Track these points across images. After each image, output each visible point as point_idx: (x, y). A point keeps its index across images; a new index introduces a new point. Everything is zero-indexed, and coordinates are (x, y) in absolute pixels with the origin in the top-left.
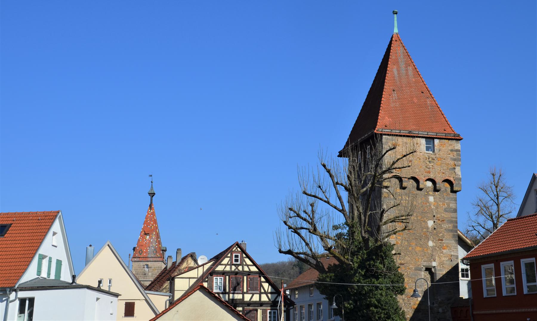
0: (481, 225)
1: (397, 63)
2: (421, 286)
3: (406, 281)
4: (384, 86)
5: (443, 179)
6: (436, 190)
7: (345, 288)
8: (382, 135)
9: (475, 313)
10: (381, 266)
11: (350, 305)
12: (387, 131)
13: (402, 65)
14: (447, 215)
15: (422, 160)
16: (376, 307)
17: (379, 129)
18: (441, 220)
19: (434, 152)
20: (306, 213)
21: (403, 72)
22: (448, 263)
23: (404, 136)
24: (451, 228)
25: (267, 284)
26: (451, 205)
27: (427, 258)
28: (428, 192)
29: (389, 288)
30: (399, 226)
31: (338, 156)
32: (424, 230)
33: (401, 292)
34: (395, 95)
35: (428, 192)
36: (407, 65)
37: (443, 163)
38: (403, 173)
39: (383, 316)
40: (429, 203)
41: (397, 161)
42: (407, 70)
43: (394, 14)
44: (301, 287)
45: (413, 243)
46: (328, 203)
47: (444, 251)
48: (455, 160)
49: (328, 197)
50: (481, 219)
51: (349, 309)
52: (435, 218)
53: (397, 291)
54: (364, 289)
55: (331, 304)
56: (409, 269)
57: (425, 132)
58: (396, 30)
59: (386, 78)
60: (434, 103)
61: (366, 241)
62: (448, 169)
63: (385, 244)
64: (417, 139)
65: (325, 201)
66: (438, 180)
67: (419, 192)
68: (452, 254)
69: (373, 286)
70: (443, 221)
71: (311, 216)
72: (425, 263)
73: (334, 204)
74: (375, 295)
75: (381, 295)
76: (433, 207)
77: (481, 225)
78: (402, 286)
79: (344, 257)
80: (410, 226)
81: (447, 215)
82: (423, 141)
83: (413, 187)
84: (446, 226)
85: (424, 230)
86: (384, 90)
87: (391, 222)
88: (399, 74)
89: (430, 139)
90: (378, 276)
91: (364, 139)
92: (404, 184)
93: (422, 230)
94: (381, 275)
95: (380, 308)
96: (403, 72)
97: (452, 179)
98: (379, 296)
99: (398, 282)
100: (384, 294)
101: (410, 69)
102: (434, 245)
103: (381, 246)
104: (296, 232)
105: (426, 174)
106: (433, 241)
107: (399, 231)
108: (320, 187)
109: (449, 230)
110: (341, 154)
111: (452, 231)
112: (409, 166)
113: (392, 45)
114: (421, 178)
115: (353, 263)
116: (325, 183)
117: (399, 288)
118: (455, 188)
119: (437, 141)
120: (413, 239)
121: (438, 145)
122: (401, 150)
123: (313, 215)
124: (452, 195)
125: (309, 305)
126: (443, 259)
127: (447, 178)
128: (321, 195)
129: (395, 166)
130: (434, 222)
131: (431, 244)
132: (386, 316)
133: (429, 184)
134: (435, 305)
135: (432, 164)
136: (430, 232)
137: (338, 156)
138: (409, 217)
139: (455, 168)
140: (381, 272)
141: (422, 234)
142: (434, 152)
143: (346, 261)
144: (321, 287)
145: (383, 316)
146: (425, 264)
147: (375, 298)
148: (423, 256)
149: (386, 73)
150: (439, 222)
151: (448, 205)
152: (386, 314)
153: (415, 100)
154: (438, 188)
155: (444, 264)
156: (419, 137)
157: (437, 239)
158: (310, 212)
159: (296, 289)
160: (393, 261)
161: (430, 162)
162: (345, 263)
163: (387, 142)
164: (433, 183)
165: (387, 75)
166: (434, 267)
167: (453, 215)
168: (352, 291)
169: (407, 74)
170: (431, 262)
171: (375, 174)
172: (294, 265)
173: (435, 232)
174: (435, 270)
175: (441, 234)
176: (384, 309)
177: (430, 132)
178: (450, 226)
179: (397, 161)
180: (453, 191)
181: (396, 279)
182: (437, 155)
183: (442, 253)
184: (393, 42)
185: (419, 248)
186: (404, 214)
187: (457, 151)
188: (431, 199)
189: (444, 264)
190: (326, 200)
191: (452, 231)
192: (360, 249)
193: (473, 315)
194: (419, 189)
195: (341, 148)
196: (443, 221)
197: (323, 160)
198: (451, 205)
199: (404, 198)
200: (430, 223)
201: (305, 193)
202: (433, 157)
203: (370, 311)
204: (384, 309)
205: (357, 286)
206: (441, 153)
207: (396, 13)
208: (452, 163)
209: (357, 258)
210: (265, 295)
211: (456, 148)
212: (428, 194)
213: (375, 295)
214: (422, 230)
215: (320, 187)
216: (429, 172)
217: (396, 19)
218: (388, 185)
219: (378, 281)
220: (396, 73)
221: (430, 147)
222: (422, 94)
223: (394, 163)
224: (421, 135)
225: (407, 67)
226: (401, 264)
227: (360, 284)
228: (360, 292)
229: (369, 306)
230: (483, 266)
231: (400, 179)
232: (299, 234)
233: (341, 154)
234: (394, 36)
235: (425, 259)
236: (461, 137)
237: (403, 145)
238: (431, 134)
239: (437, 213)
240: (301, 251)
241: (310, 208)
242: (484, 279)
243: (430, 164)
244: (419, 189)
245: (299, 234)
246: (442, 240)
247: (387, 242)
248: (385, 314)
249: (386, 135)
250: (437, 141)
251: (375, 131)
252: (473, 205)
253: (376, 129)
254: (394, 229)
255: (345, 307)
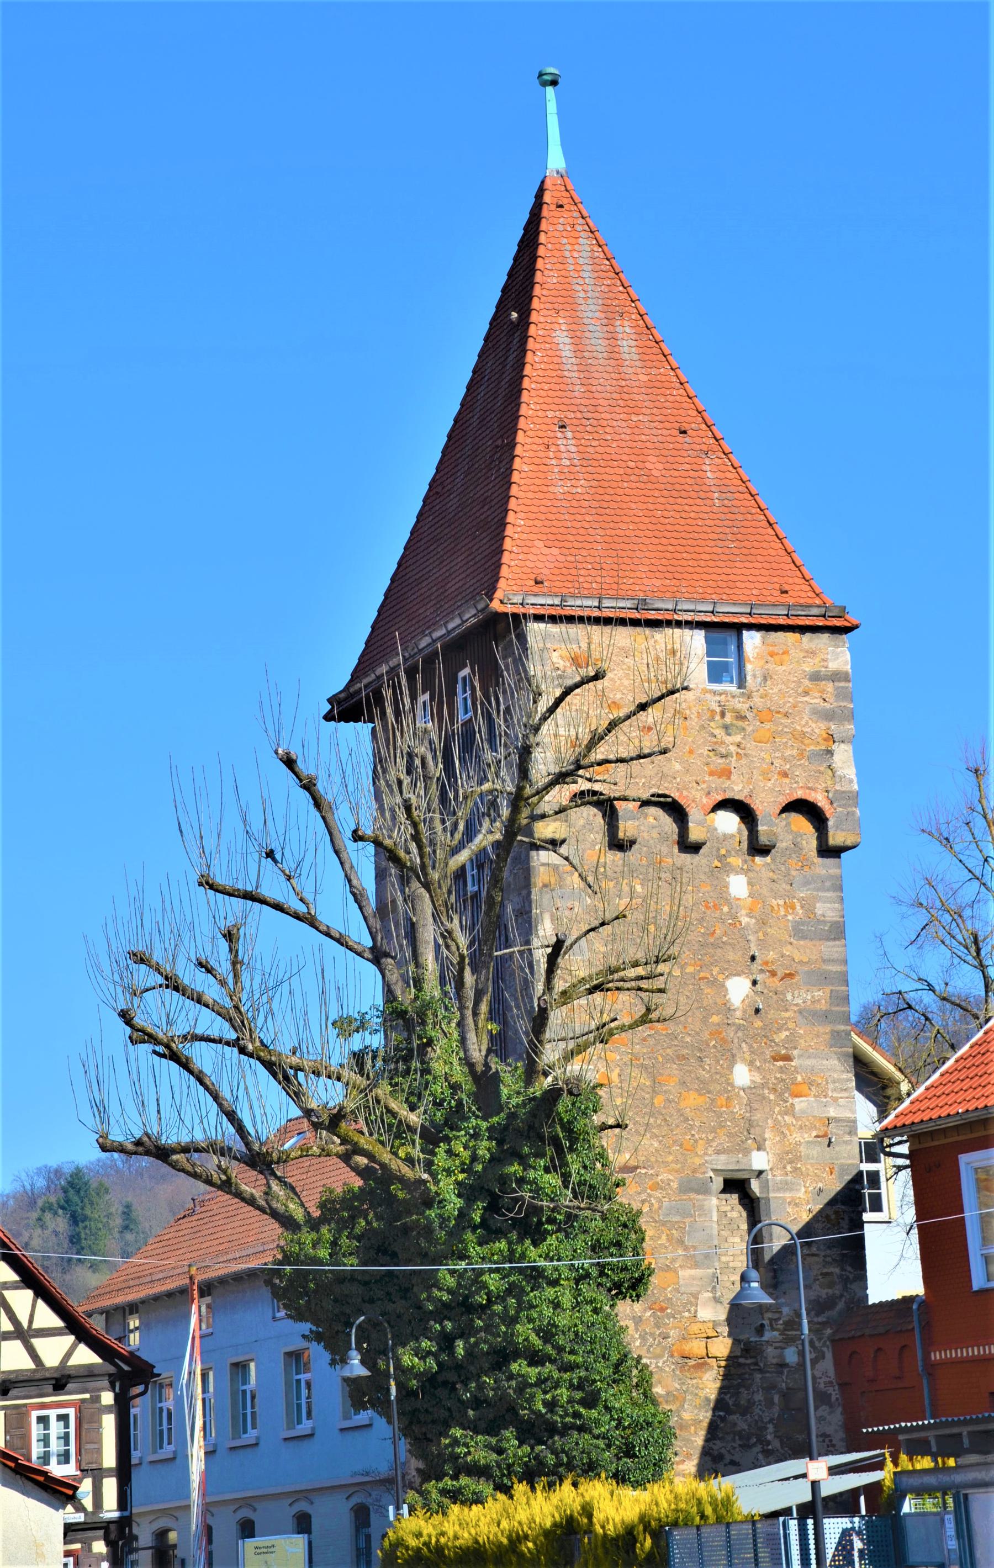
0: (931, 988)
1: (567, 303)
2: (707, 1256)
3: (648, 1235)
4: (518, 405)
5: (784, 801)
6: (758, 848)
7: (405, 1288)
8: (518, 619)
9: (936, 1356)
10: (553, 1180)
11: (423, 1358)
12: (544, 601)
13: (591, 311)
14: (804, 953)
15: (694, 722)
16: (535, 1359)
17: (509, 596)
18: (780, 974)
19: (742, 684)
20: (209, 971)
21: (597, 342)
22: (815, 1152)
23: (622, 622)
24: (823, 1006)
25: (29, 1294)
26: (820, 908)
27: (730, 1135)
28: (721, 858)
29: (587, 1275)
30: (624, 1005)
31: (328, 717)
32: (715, 1019)
33: (634, 1287)
34: (567, 443)
35: (721, 858)
36: (611, 315)
37: (781, 734)
38: (608, 782)
39: (563, 1394)
40: (728, 902)
41: (609, 730)
42: (612, 337)
43: (544, 84)
44: (156, 1298)
45: (672, 1074)
46: (311, 921)
47: (800, 1104)
48: (829, 716)
49: (309, 897)
50: (934, 962)
51: (418, 1376)
52: (756, 966)
53: (617, 1285)
54: (484, 1286)
55: (340, 1358)
56: (656, 1187)
57: (703, 601)
58: (556, 160)
59: (527, 370)
60: (732, 475)
61: (486, 1083)
62: (801, 755)
63: (574, 1089)
64: (669, 631)
65: (297, 916)
66: (766, 805)
67: (687, 858)
68: (832, 1113)
69: (521, 1271)
70: (790, 975)
71: (230, 981)
72: (723, 1157)
73: (338, 927)
74: (532, 1307)
75: (556, 1305)
76: (745, 920)
77: (931, 988)
78: (638, 1265)
79: (395, 1154)
80: (665, 1004)
81: (804, 953)
82: (698, 639)
83: (663, 838)
84: (805, 996)
85: (715, 1019)
86: (522, 423)
87: (591, 991)
88: (578, 350)
89: (723, 632)
90: (540, 1223)
91: (442, 641)
92: (626, 828)
93: (705, 1020)
94: (551, 1221)
95: (552, 1361)
96: (597, 342)
97: (820, 799)
98: (548, 1311)
99: (618, 1244)
100: (567, 1300)
101: (625, 328)
102: (758, 1078)
103: (553, 1095)
104: (174, 1056)
105: (715, 782)
106: (751, 1063)
107: (622, 1029)
108: (270, 854)
109: (814, 1014)
110: (346, 708)
111: (825, 1017)
112: (664, 752)
113: (544, 225)
114: (697, 803)
115: (434, 1175)
116: (293, 834)
117: (625, 1269)
118: (836, 838)
119: (752, 640)
120: (668, 1059)
121: (759, 657)
122: (622, 687)
123: (236, 976)
124: (826, 867)
125: (236, 1365)
126: (796, 1137)
127: (800, 794)
128: (274, 888)
129: (600, 753)
130: (755, 983)
131: (742, 1075)
132: (578, 1395)
133: (729, 822)
134: (768, 1335)
135: (738, 738)
136: (739, 1027)
137: (328, 717)
138: (662, 968)
139: (830, 753)
140: (553, 1210)
141: (705, 1035)
142: (742, 684)
143: (406, 1171)
144: (292, 1287)
145: (563, 1394)
146: (727, 1162)
147: (530, 1320)
148: (713, 1130)
149: (524, 351)
150: (775, 983)
151: (809, 908)
152: (580, 1387)
153: (655, 466)
154: (763, 839)
155: (798, 1158)
156: (679, 624)
157: (768, 1053)
158: (224, 967)
159: (133, 1308)
160: (602, 1156)
161: (726, 727)
162: (402, 1180)
163: (550, 652)
164: (743, 819)
165: (529, 357)
166: (760, 1173)
167: (831, 949)
168: (429, 1298)
169: (613, 353)
170: (747, 1152)
171: (520, 789)
172: (48, 1208)
173: (758, 1024)
174: (765, 1186)
175: (784, 1034)
176: (569, 1367)
177: (722, 601)
178: (819, 996)
179: (609, 730)
180: (828, 851)
181: (610, 1235)
182: (757, 701)
183: (790, 1111)
184: (545, 212)
185: (693, 1095)
186: (640, 955)
187: (836, 677)
188: (738, 886)
189: (798, 1158)
190: (302, 909)
191: (825, 1017)
192: (456, 1116)
193: (931, 1368)
194: (689, 847)
195: (338, 680)
196: (790, 975)
197: (285, 735)
198: (820, 908)
199: (626, 883)
200: (738, 990)
201: (208, 884)
202: (741, 705)
203: (511, 1377)
204: (569, 1367)
205: (452, 1272)
206: (773, 690)
207: (554, 83)
208: (818, 728)
209: (450, 1152)
210: (17, 1345)
211: (833, 666)
212: (726, 868)
213: (532, 1307)
214: (705, 1020)
215: (270, 854)
216: (726, 773)
217: (552, 107)
218: (559, 836)
219: (544, 1247)
220: (567, 352)
221: (725, 667)
222: (681, 438)
223: (596, 740)
224: (688, 617)
225: (609, 322)
226: (627, 1169)
227: (462, 1265)
228: (466, 1297)
229: (502, 1357)
230: (964, 1159)
231: (607, 807)
232: (185, 1064)
233: (346, 708)
234: (548, 184)
235: (722, 1140)
236: (853, 618)
237: (632, 659)
238: (729, 611)
239: (762, 943)
240: (199, 1136)
241: (224, 945)
242: (970, 1214)
243: (729, 739)
244: (689, 847)
245: (185, 1064)
246: (787, 1058)
247: (579, 1079)
248: (571, 1387)
249: (539, 618)
250: (752, 640)
251: (496, 605)
252: (899, 902)
253: (499, 594)
254: (606, 1018)
255: (398, 1366)
